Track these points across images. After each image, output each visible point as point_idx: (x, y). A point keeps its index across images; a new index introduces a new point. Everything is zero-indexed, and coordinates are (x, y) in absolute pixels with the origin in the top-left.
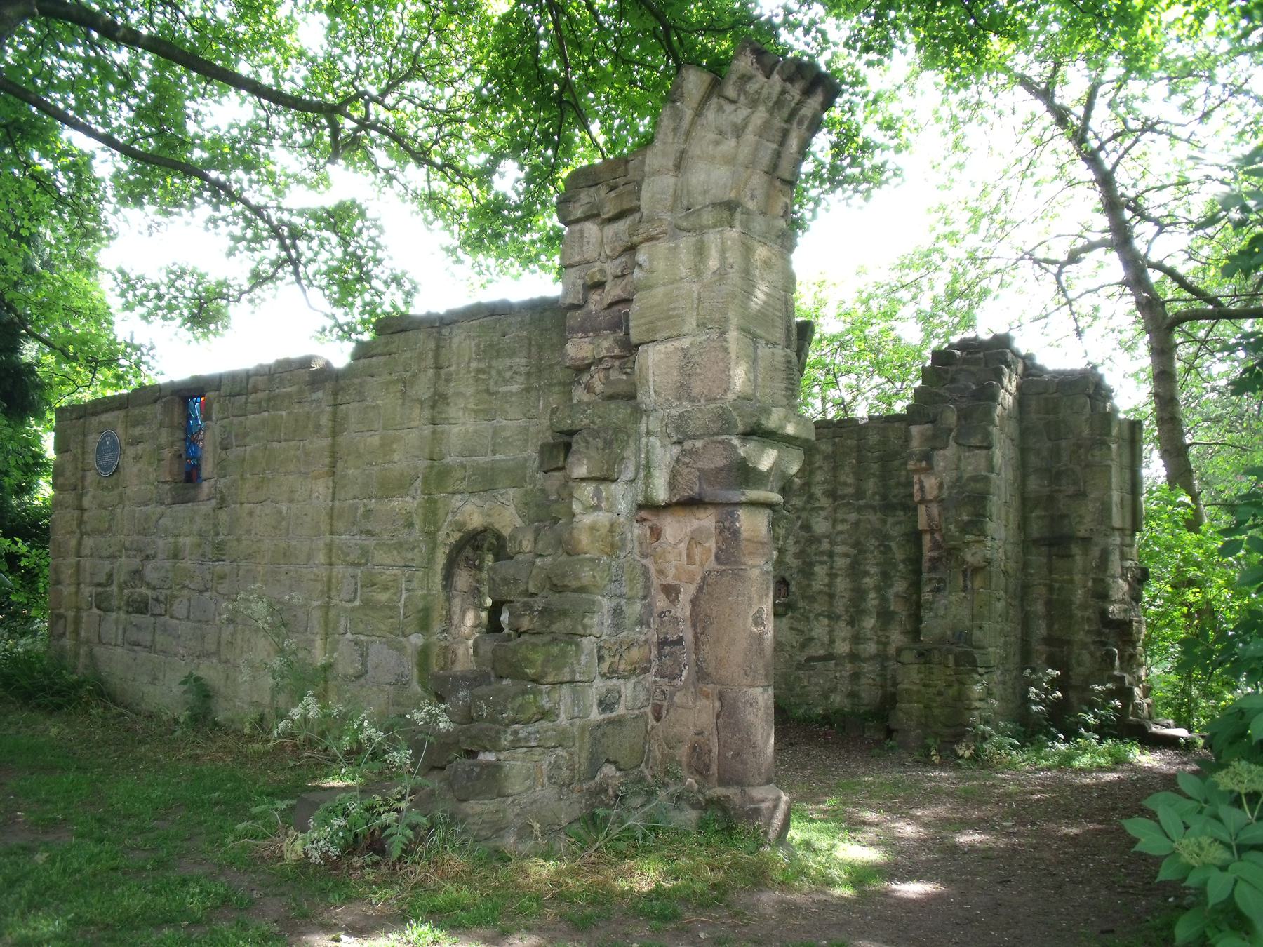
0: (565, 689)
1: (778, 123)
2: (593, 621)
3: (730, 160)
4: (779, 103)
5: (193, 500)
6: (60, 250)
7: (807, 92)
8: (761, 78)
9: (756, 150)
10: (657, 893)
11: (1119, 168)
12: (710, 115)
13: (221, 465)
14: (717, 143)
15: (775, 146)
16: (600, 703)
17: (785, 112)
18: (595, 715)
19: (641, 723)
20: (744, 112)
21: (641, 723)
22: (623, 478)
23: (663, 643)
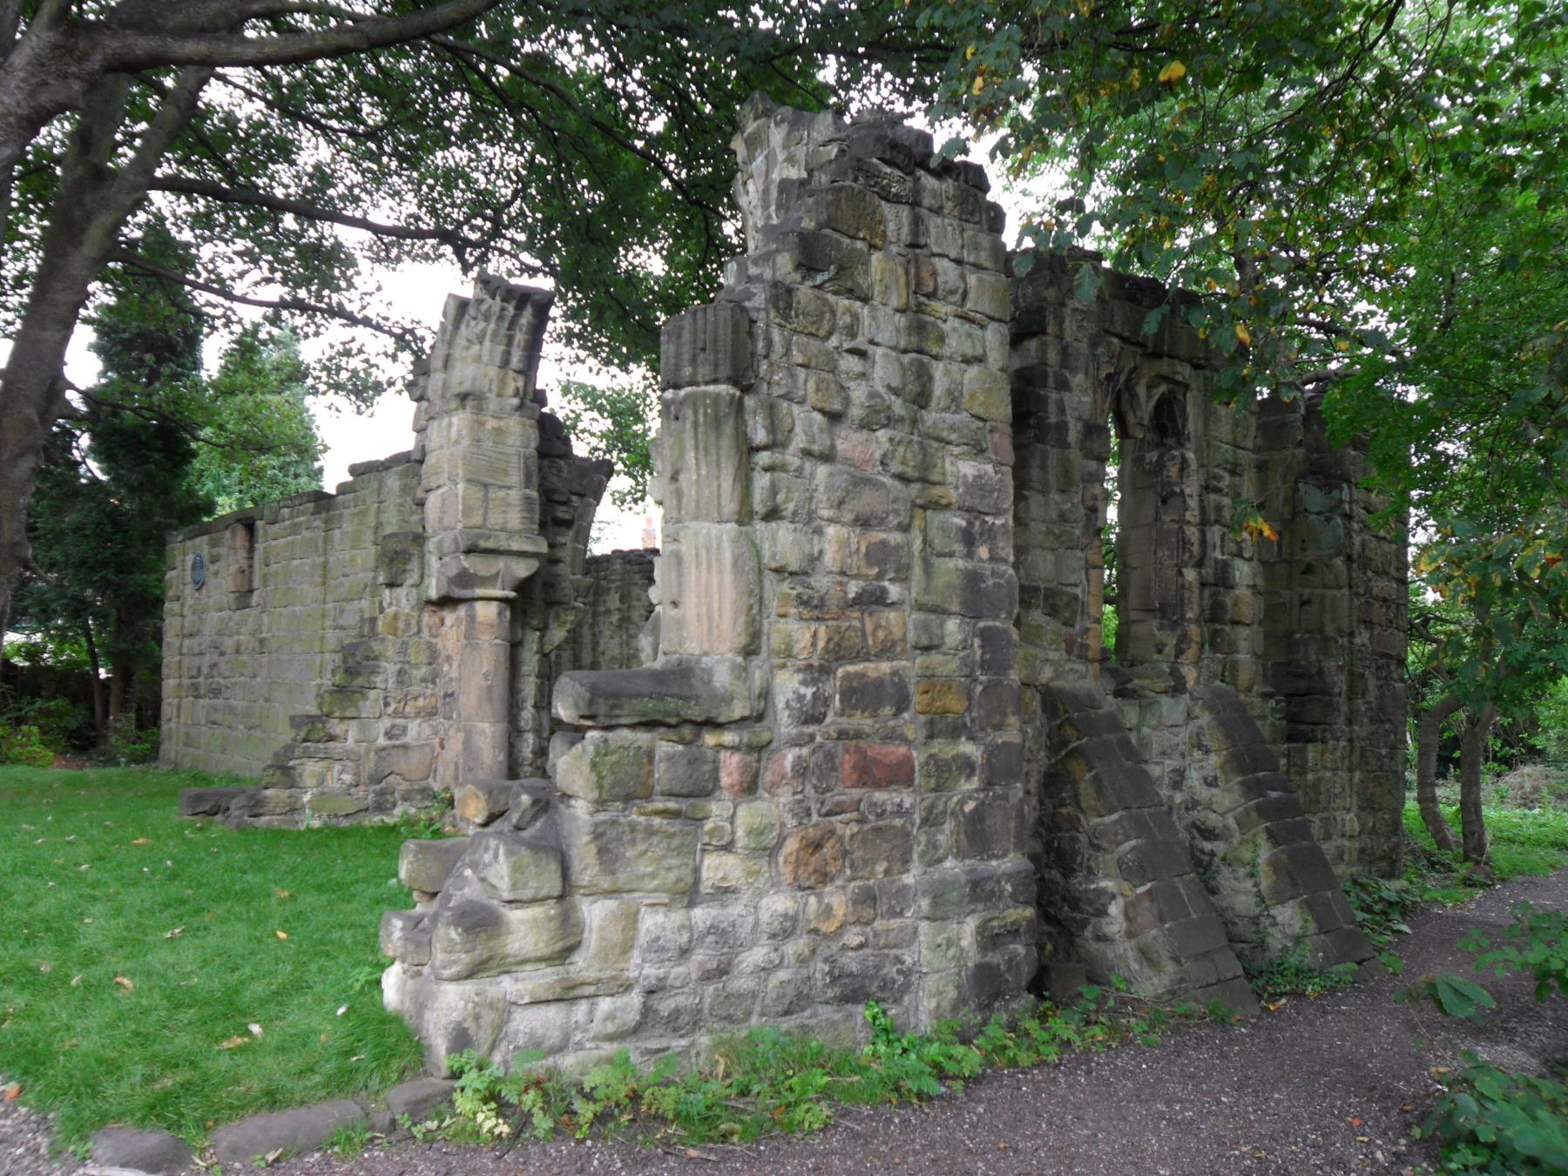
0: (353, 724)
1: (503, 331)
2: (378, 680)
3: (478, 359)
4: (501, 318)
5: (248, 606)
6: (432, 188)
7: (520, 308)
8: (490, 301)
9: (491, 351)
10: (1195, 452)
11: (544, 892)
12: (463, 330)
13: (265, 578)
14: (468, 348)
15: (502, 348)
16: (386, 734)
17: (506, 324)
18: (382, 741)
19: (427, 749)
20: (482, 325)
21: (427, 749)
22: (410, 582)
23: (446, 695)
